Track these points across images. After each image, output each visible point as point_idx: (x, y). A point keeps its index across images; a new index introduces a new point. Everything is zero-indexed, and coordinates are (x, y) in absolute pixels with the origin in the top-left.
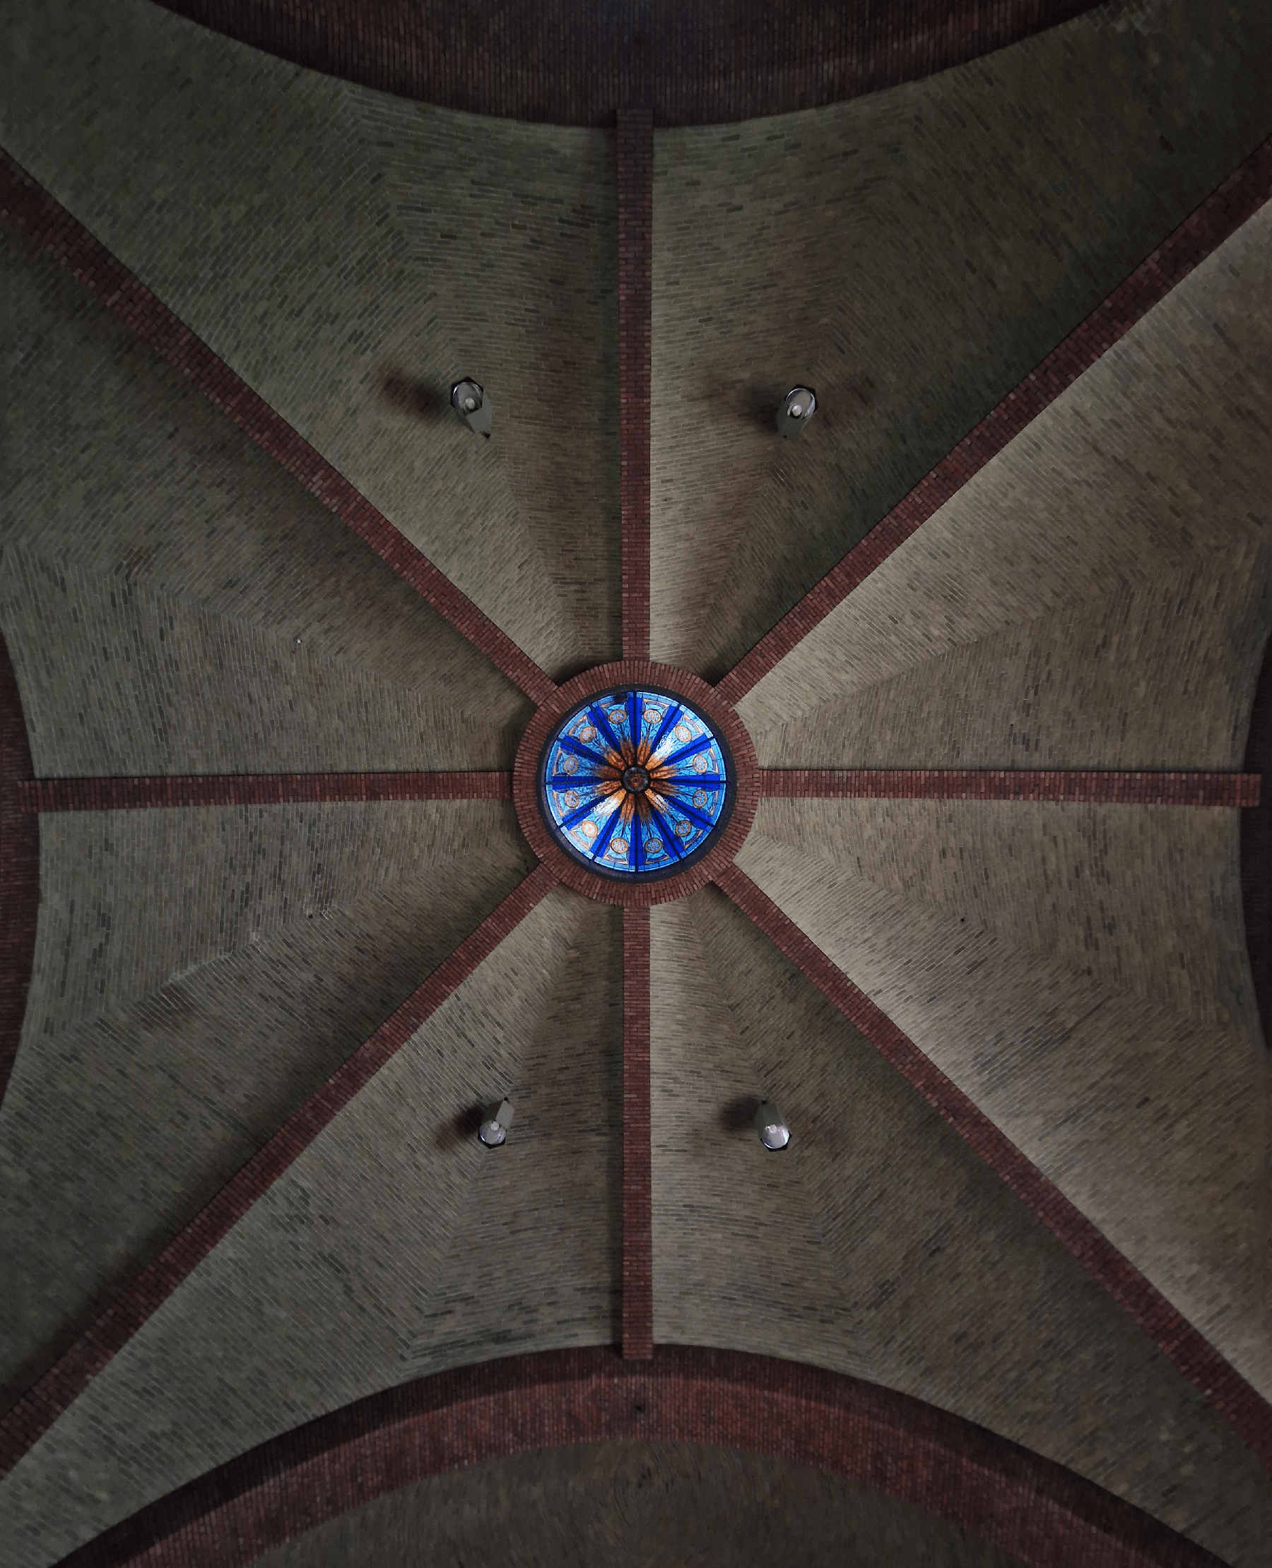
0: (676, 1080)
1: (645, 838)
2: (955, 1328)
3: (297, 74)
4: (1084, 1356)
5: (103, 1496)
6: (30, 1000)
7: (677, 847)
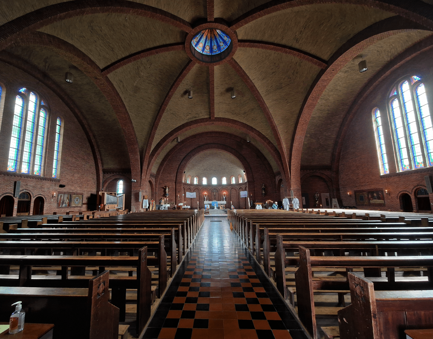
1: (213, 45)
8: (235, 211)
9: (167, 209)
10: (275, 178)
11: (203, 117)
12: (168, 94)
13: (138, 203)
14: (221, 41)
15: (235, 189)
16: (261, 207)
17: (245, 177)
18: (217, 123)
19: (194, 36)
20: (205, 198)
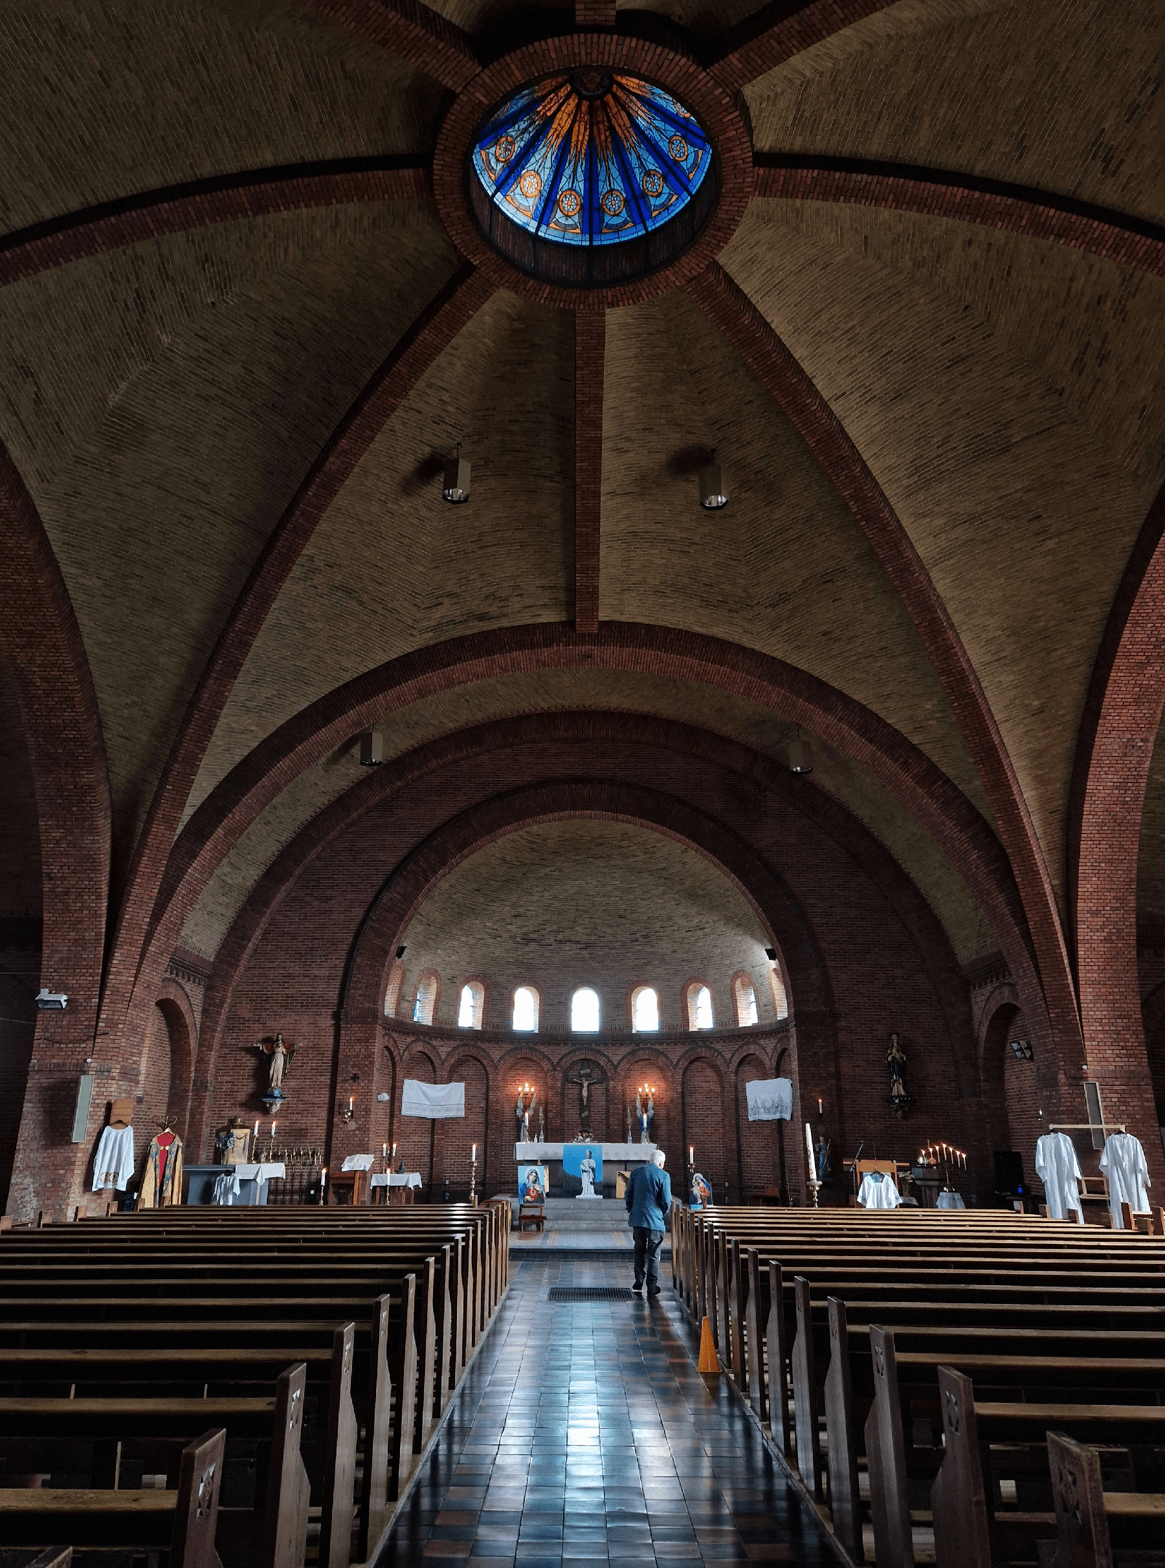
0: (627, 439)
1: (603, 188)
2: (824, 628)
3: (625, 1231)
4: (902, 660)
5: (253, 728)
6: (17, 464)
7: (644, 210)
8: (713, 1215)
9: (260, 1198)
10: (967, 1000)
11: (527, 619)
12: (316, 468)
13: (60, 1154)
14: (651, 164)
15: (715, 1067)
16: (893, 1191)
17: (778, 990)
18: (611, 653)
19: (487, 130)
20: (519, 1121)
